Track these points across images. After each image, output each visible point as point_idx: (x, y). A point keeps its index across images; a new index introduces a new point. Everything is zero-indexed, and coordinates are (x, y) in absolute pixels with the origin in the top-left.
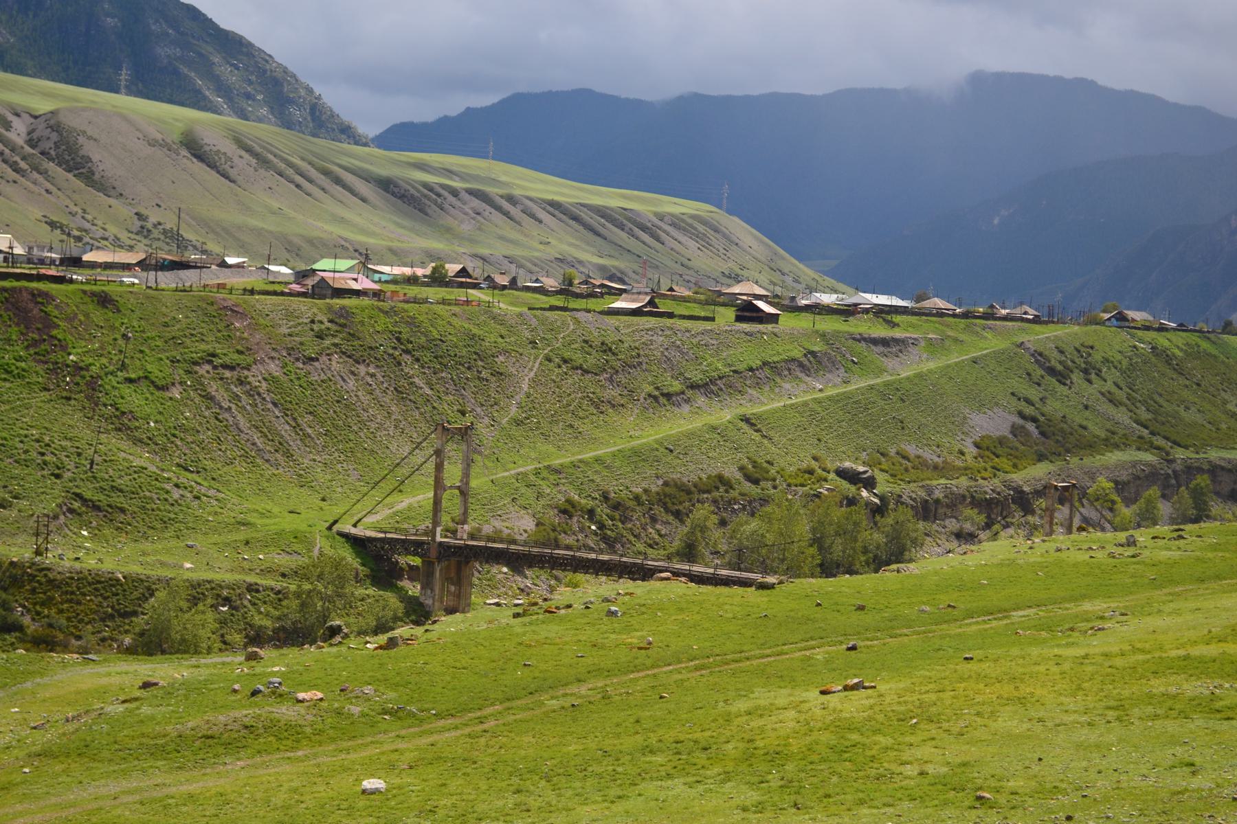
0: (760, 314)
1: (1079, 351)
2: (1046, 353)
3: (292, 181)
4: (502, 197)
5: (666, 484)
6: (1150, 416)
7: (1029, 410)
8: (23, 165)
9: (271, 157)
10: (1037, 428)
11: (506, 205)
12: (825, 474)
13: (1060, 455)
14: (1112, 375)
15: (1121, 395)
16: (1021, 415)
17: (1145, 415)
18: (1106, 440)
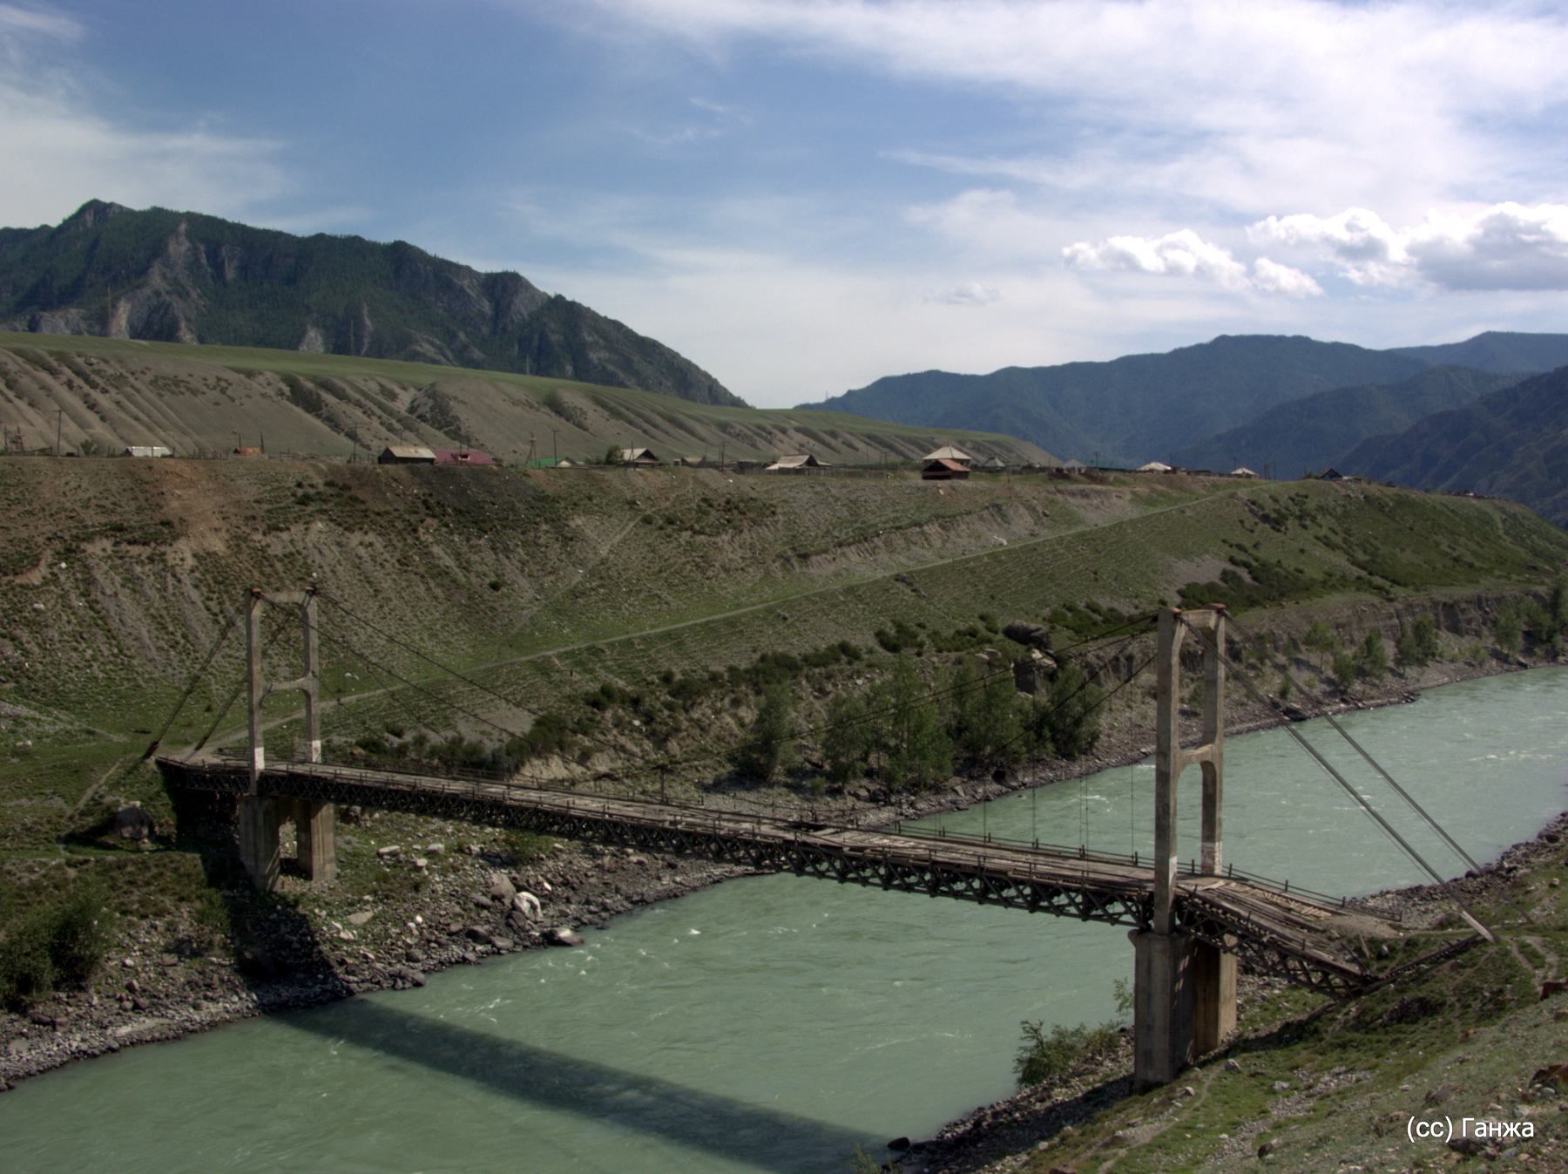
0: (948, 473)
1: (1293, 500)
2: (1261, 502)
3: (639, 427)
4: (825, 432)
5: (763, 658)
6: (1367, 558)
7: (1241, 557)
8: (397, 426)
9: (623, 410)
10: (1250, 573)
11: (828, 439)
12: (990, 635)
13: (1274, 600)
14: (1326, 522)
15: (1338, 540)
16: (1232, 561)
17: (1361, 557)
18: (1324, 582)
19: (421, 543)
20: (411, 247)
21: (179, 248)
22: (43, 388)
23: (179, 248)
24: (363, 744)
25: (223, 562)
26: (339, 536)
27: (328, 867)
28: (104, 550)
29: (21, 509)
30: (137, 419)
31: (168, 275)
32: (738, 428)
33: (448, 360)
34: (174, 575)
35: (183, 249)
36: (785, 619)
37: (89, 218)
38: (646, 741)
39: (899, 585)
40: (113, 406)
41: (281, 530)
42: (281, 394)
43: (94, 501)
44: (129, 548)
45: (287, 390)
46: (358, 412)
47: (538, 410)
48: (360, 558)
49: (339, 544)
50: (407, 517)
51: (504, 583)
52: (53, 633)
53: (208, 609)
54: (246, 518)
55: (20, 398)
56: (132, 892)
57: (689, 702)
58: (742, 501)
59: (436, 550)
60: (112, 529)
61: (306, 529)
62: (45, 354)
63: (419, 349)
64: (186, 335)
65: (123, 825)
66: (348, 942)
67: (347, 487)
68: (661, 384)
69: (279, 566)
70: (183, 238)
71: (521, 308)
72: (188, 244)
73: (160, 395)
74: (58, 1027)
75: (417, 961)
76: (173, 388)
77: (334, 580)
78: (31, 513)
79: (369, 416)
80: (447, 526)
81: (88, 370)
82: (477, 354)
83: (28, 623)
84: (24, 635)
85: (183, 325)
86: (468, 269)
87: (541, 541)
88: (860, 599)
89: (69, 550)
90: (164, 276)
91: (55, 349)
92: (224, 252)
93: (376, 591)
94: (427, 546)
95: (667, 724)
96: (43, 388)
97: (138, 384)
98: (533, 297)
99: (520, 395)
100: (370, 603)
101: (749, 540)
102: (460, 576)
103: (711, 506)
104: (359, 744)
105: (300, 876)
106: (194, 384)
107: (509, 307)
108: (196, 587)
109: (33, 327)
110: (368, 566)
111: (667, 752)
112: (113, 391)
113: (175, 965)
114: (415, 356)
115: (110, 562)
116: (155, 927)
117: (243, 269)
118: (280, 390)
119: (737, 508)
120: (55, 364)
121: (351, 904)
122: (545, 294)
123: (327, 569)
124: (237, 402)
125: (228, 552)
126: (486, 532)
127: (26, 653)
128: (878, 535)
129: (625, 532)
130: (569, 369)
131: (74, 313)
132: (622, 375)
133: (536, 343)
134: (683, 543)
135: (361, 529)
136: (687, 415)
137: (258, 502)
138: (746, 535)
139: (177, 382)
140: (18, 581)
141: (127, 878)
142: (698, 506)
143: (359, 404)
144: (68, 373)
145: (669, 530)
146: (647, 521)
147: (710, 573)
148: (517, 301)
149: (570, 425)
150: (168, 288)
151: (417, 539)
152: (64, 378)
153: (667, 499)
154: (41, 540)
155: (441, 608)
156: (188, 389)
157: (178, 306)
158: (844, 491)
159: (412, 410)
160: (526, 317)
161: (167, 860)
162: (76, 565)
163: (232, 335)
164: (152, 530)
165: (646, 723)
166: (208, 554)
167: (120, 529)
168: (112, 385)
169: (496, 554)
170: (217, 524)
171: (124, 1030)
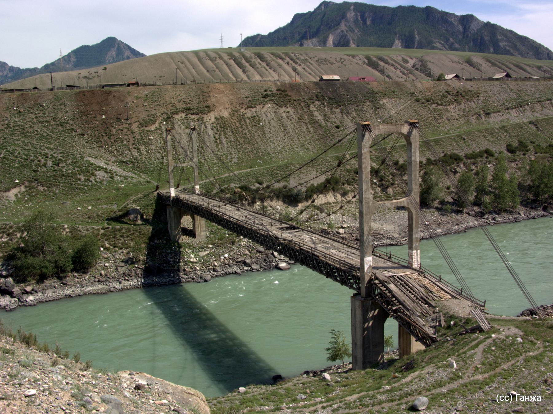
5: (445, 155)
8: (406, 72)
9: (497, 63)
19: (310, 111)
20: (432, 8)
21: (351, 15)
22: (279, 65)
23: (351, 15)
24: (241, 188)
25: (226, 120)
26: (276, 109)
27: (202, 233)
28: (181, 117)
29: (156, 104)
30: (310, 74)
31: (347, 25)
32: (545, 68)
33: (446, 49)
34: (205, 125)
35: (352, 15)
36: (464, 139)
37: (323, 7)
38: (378, 188)
39: (530, 126)
40: (302, 70)
41: (253, 108)
42: (364, 63)
43: (183, 100)
44: (191, 116)
45: (366, 61)
46: (392, 68)
47: (462, 64)
48: (282, 117)
49: (275, 112)
50: (307, 101)
51: (342, 126)
52: (153, 147)
53: (214, 137)
54: (240, 104)
55: (271, 69)
56: (121, 240)
57: (403, 173)
58: (464, 92)
59: (316, 113)
60: (186, 110)
61: (263, 107)
62: (281, 54)
63: (435, 45)
64: (352, 45)
65: (130, 214)
66: (193, 262)
67: (285, 91)
68: (528, 53)
69: (248, 121)
70: (352, 11)
71: (474, 27)
72: (354, 13)
73: (319, 65)
74: (67, 286)
75: (217, 271)
76: (324, 62)
77: (268, 126)
78: (159, 105)
79: (396, 69)
80: (324, 104)
81: (295, 58)
82: (457, 46)
83: (145, 144)
84: (142, 148)
85: (351, 42)
86: (454, 14)
87: (364, 109)
88: (506, 131)
89: (168, 118)
90: (346, 25)
91: (284, 51)
92: (366, 15)
93: (285, 129)
94: (312, 112)
95: (389, 181)
96: (279, 65)
97: (312, 62)
98: (478, 23)
99: (456, 59)
100: (281, 134)
101: (463, 107)
102: (323, 123)
103: (449, 94)
104: (239, 187)
105: (191, 237)
106: (332, 61)
107: (469, 28)
108: (212, 129)
109: (301, 45)
110: (285, 120)
111: (386, 193)
112: (303, 65)
113: (123, 267)
114: (433, 48)
115: (182, 121)
116: (122, 252)
117: (373, 21)
118: (364, 61)
119: (461, 94)
120: (284, 56)
121: (203, 248)
122: (483, 22)
123: (267, 122)
124: (347, 66)
125: (229, 116)
126: (340, 106)
127: (141, 154)
128: (528, 105)
129: (405, 105)
130: (492, 50)
131: (314, 40)
132: (512, 51)
133: (479, 40)
134: (431, 109)
135: (286, 106)
136: (525, 64)
137: (246, 97)
138: (462, 106)
139: (326, 60)
140: (146, 129)
141: (121, 234)
142: (443, 94)
143: (393, 65)
144: (288, 59)
145: (427, 104)
146: (417, 100)
147: (440, 121)
148: (472, 25)
149: (475, 70)
150: (347, 29)
151: (309, 109)
152: (286, 61)
153: (430, 92)
154: (158, 114)
155: (310, 136)
156: (329, 63)
157: (350, 36)
158: (517, 87)
159: (413, 66)
160: (476, 31)
161: (138, 229)
162: (170, 123)
163: (369, 44)
164: (201, 109)
165: (380, 181)
166: (221, 117)
167: (189, 109)
168: (303, 63)
169: (342, 114)
170: (227, 106)
171: (88, 289)
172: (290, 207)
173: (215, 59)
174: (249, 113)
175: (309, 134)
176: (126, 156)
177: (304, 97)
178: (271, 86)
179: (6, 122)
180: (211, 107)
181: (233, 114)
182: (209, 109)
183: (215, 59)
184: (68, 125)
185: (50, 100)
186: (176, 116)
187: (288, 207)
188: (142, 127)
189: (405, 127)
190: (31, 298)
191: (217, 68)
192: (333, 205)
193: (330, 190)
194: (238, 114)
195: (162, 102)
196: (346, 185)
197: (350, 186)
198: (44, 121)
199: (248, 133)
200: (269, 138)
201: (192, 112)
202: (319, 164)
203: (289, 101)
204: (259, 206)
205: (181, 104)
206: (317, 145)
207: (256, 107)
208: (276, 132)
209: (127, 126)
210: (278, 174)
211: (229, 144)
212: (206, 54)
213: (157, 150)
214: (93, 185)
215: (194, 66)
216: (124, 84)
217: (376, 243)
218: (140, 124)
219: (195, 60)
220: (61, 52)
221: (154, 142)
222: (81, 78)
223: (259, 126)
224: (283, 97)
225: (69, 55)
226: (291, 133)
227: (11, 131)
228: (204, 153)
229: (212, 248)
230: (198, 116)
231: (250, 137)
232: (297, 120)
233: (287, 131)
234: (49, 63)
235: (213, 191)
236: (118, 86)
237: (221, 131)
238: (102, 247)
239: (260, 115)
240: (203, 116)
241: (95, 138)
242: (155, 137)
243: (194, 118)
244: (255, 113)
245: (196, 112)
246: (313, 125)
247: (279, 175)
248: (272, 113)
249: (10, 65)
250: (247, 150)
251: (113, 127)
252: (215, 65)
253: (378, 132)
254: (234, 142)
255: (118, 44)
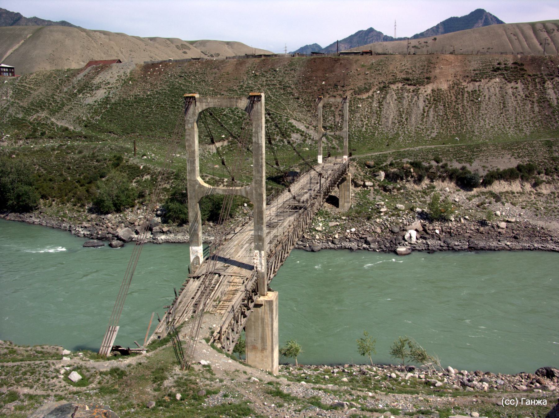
25: (442, 93)
27: (346, 204)
29: (378, 72)
41: (477, 81)
49: (501, 88)
52: (358, 115)
61: (489, 81)
69: (466, 95)
75: (335, 244)
78: (380, 74)
93: (504, 107)
100: (497, 112)
105: (335, 206)
108: (424, 101)
123: (487, 97)
135: (515, 82)
137: (474, 70)
151: (543, 86)
155: (533, 115)
164: (421, 80)
166: (438, 90)
167: (408, 80)
170: (450, 78)
172: (462, 190)
173: (552, 31)
174: (471, 87)
175: (531, 113)
176: (328, 122)
177: (543, 72)
178: (508, 59)
179: (242, 84)
180: (432, 79)
181: (453, 87)
182: (429, 80)
183: (552, 31)
184: (290, 89)
185: (285, 65)
186: (392, 86)
187: (459, 190)
188: (355, 95)
189: (243, 101)
190: (163, 237)
191: (553, 40)
192: (516, 194)
193: (518, 178)
194: (458, 88)
195: (384, 72)
196: (542, 175)
197: (548, 177)
198: (271, 84)
199: (461, 108)
200: (483, 115)
201: (410, 83)
202: (520, 148)
203: (522, 76)
204: (426, 185)
205: (402, 73)
206: (536, 126)
207: (481, 81)
208: (493, 109)
209: (341, 93)
210: (464, 153)
211: (436, 118)
212: (544, 26)
213: (361, 118)
214: (283, 146)
215: (526, 38)
216: (359, 53)
217: (536, 245)
218: (354, 92)
219: (530, 33)
220: (395, 23)
221: (361, 110)
222: (411, 47)
223: (477, 101)
224: (517, 71)
225: (437, 27)
226: (510, 111)
227: (242, 92)
228: (406, 125)
229: (345, 220)
230: (415, 87)
231: (462, 112)
232: (524, 97)
233: (506, 109)
234: (419, 33)
235: (382, 164)
236: (353, 54)
237: (432, 104)
238: (246, 203)
239: (482, 90)
240: (419, 87)
241: (308, 102)
242: (364, 106)
243: (410, 89)
244: (477, 87)
245: (414, 83)
246: (541, 104)
247: (465, 155)
248: (497, 89)
249: (385, 34)
250: (451, 126)
251: (327, 93)
252: (551, 38)
253: (206, 106)
254: (442, 116)
255: (486, 16)
